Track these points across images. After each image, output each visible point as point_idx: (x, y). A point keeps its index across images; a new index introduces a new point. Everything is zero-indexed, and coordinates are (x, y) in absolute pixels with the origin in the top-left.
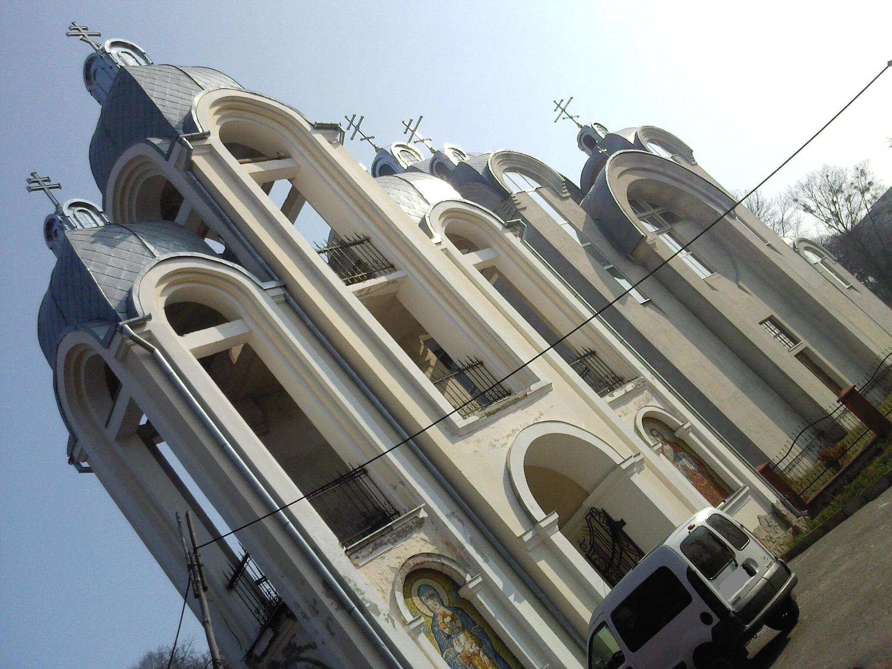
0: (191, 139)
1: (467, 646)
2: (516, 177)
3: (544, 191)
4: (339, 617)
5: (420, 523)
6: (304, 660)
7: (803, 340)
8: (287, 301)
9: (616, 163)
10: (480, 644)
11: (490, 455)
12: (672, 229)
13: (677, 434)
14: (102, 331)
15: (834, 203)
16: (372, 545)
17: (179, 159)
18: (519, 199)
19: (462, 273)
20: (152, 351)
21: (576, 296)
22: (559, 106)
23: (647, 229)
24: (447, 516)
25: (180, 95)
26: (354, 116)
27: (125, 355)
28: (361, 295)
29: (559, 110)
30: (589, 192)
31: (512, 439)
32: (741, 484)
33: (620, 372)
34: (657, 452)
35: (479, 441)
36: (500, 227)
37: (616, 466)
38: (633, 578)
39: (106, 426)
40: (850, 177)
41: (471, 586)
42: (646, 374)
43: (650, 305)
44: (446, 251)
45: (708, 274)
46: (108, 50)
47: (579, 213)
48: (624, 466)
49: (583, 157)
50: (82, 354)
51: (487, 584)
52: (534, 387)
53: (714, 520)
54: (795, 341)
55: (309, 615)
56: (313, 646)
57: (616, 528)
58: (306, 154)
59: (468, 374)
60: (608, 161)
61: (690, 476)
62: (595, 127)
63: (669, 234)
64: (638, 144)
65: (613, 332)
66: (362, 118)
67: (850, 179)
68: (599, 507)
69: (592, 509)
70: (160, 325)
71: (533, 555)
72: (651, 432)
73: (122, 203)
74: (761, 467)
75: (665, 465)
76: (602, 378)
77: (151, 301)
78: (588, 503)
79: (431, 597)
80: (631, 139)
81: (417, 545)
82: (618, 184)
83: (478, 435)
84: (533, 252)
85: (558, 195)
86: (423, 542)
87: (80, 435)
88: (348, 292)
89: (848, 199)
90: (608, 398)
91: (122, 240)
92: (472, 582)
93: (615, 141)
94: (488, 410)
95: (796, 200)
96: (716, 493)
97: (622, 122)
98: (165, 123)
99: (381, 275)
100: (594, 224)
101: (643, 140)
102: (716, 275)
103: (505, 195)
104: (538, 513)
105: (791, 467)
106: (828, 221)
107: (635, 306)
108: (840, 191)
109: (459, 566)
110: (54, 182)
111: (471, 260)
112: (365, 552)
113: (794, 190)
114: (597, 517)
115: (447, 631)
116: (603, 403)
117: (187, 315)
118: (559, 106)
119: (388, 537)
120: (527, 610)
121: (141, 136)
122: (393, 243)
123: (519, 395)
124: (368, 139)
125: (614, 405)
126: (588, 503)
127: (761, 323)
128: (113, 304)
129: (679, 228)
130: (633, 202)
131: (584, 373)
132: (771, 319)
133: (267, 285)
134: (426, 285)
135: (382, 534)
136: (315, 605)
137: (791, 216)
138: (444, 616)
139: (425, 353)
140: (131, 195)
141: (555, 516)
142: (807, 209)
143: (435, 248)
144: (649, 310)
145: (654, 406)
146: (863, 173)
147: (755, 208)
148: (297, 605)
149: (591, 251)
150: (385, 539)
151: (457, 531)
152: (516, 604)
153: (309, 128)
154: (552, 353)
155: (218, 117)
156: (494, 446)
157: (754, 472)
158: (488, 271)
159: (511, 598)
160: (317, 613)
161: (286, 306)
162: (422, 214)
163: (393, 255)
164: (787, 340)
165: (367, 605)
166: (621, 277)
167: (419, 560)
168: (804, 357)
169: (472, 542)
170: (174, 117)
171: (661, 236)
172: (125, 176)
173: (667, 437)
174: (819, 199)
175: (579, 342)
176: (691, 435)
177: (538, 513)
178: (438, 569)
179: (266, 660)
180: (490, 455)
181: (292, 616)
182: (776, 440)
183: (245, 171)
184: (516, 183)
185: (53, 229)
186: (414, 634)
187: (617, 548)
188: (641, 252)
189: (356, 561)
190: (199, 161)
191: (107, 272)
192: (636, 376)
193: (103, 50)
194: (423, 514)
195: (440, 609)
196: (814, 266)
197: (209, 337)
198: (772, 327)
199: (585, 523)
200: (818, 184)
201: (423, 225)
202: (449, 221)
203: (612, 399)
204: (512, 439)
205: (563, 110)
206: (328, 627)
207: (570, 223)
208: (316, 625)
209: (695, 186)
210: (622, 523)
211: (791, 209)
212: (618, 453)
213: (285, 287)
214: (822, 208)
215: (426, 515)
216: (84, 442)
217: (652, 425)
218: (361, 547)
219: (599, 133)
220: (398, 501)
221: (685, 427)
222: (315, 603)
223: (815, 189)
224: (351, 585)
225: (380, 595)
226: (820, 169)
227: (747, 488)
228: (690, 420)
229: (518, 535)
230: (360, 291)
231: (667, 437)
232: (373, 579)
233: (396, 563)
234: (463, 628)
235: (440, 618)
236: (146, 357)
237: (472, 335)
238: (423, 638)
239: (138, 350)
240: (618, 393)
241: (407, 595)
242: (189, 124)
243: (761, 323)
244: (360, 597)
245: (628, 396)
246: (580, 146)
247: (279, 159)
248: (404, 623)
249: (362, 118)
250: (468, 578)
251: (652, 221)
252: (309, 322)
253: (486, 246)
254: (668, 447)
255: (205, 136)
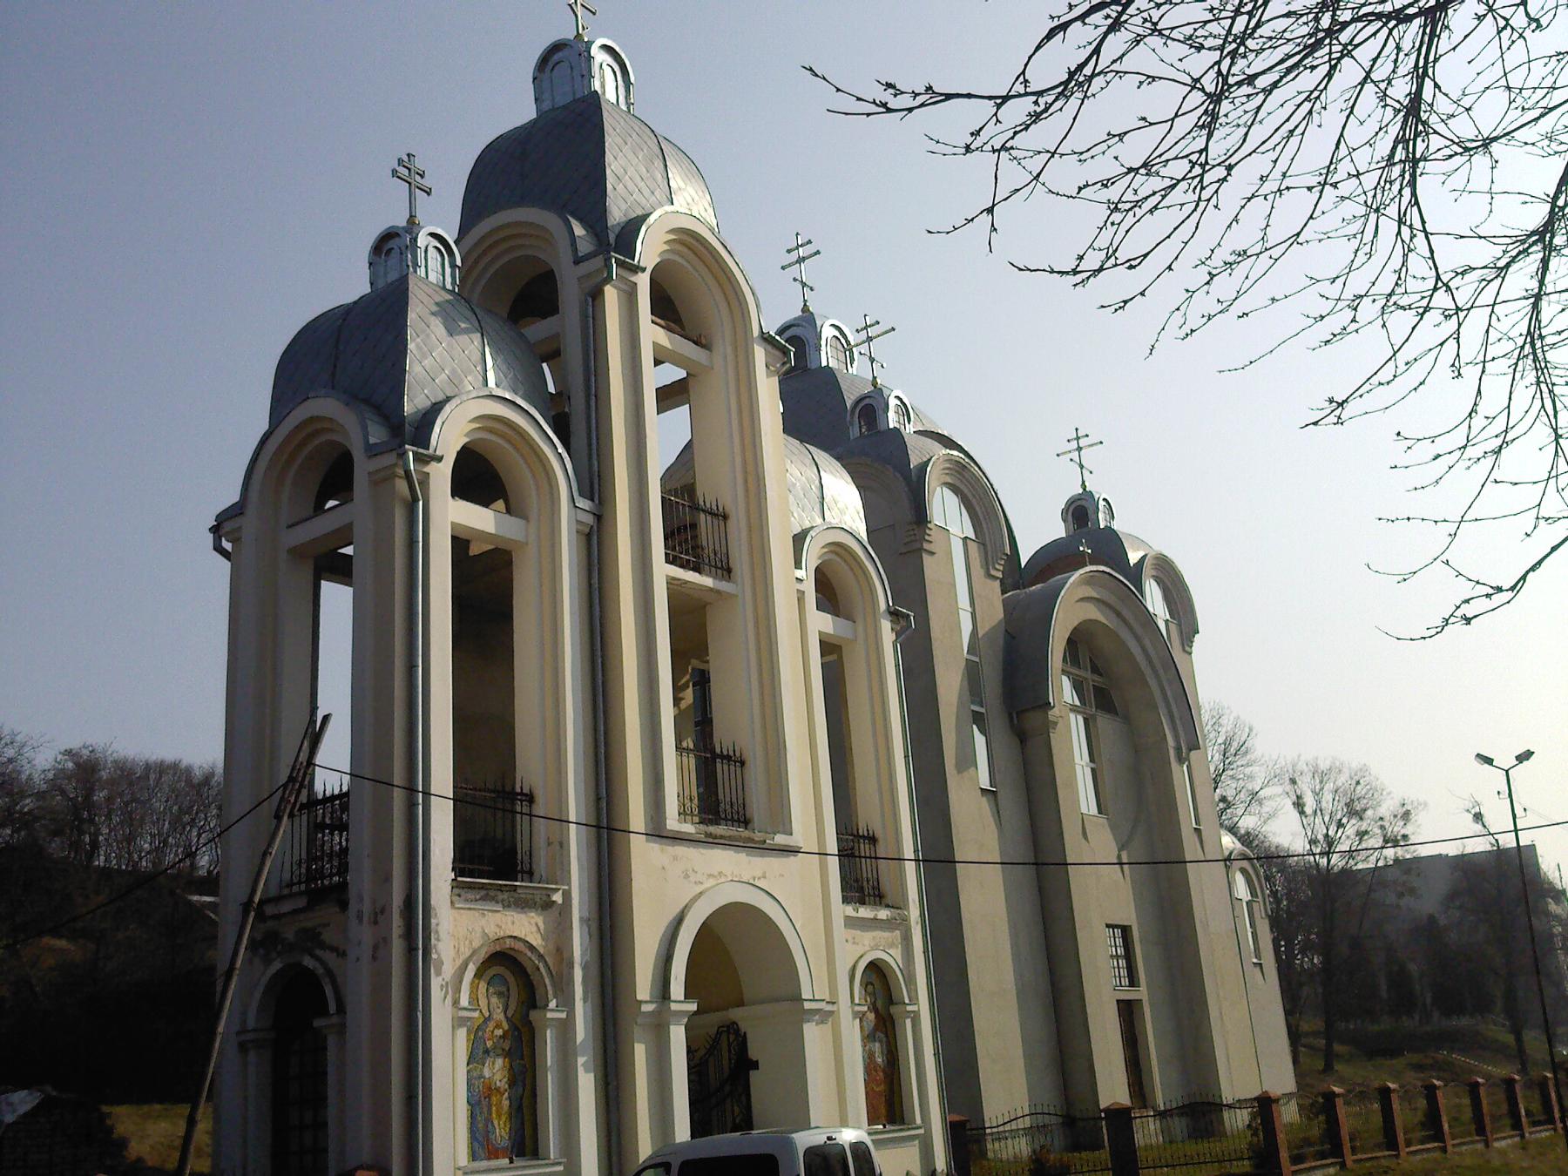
0: (620, 264)
1: (498, 1077)
2: (952, 500)
3: (973, 547)
4: (397, 947)
5: (548, 905)
6: (318, 959)
7: (1143, 988)
8: (589, 536)
9: (1090, 580)
10: (512, 1083)
11: (679, 883)
12: (1093, 717)
13: (893, 1009)
14: (377, 434)
15: (1340, 825)
16: (483, 893)
17: (589, 275)
18: (934, 534)
19: (798, 626)
20: (415, 500)
21: (906, 757)
22: (1078, 438)
23: (1063, 691)
24: (581, 919)
25: (642, 184)
26: (810, 242)
27: (382, 480)
28: (672, 582)
29: (1074, 445)
30: (1027, 581)
31: (712, 882)
32: (919, 1121)
33: (886, 886)
34: (855, 1014)
35: (675, 858)
36: (883, 606)
37: (798, 999)
38: (726, 1143)
39: (289, 527)
40: (1386, 808)
41: (549, 1015)
42: (914, 913)
43: (991, 796)
44: (801, 595)
45: (1094, 810)
46: (594, 50)
47: (994, 612)
48: (807, 1005)
49: (1056, 530)
50: (331, 430)
51: (567, 1026)
52: (780, 839)
53: (860, 1150)
54: (1133, 982)
55: (365, 919)
56: (342, 954)
57: (745, 1064)
58: (730, 358)
59: (719, 766)
60: (1082, 571)
61: (870, 1067)
62: (1102, 503)
63: (1086, 721)
64: (1136, 574)
65: (914, 833)
66: (818, 253)
67: (1384, 810)
68: (743, 1027)
69: (734, 1023)
70: (441, 475)
71: (637, 1030)
72: (866, 984)
73: (485, 253)
74: (957, 1118)
75: (852, 1035)
76: (862, 882)
77: (449, 437)
78: (736, 1014)
79: (500, 994)
80: (1133, 557)
81: (526, 927)
82: (1073, 604)
83: (681, 850)
84: (897, 665)
85: (987, 565)
86: (534, 929)
87: (251, 510)
88: (663, 571)
89: (1362, 835)
90: (849, 910)
91: (466, 331)
92: (553, 1011)
93: (1109, 547)
94: (712, 829)
95: (1293, 781)
96: (883, 1110)
97: (1141, 527)
98: (603, 212)
99: (709, 575)
100: (1001, 641)
101: (1148, 570)
102: (1103, 820)
103: (920, 516)
104: (677, 989)
105: (999, 1137)
106: (1313, 842)
107: (975, 770)
108: (1359, 815)
109: (554, 985)
110: (426, 182)
111: (822, 623)
112: (470, 896)
113: (1301, 766)
114: (732, 1037)
115: (489, 1044)
116: (841, 910)
117: (477, 477)
118: (1078, 438)
119: (506, 895)
120: (587, 1085)
121: (564, 209)
122: (751, 546)
123: (758, 836)
124: (804, 285)
125: (851, 922)
126: (736, 1014)
127: (1108, 926)
128: (408, 408)
129: (1104, 722)
130: (1072, 642)
131: (847, 854)
132: (1126, 931)
133: (583, 503)
134: (751, 625)
135: (500, 888)
136: (380, 913)
137: (1270, 798)
138: (498, 1026)
139: (686, 686)
140: (498, 257)
141: (693, 1007)
142: (1299, 805)
143: (791, 582)
144: (984, 802)
145: (893, 958)
146: (1406, 816)
147: (1232, 750)
148: (361, 899)
149: (973, 673)
150: (501, 896)
151: (579, 944)
152: (581, 1070)
153: (756, 333)
154: (834, 863)
155: (666, 247)
156: (687, 876)
157: (944, 1119)
158: (829, 648)
159: (581, 1060)
160: (376, 923)
161: (583, 538)
162: (807, 525)
163: (740, 559)
164: (1124, 972)
165: (434, 956)
166: (983, 731)
167: (519, 946)
168: (1128, 1011)
169: (585, 968)
170: (617, 212)
171: (1072, 716)
172: (515, 231)
173: (879, 1004)
174: (1324, 805)
175: (868, 816)
176: (908, 1022)
177: (677, 989)
178: (529, 971)
179: (270, 924)
180: (679, 883)
181: (344, 905)
182: (1009, 1092)
183: (652, 334)
184: (947, 513)
185: (391, 247)
186: (459, 1022)
187: (727, 1088)
188: (1032, 720)
189: (456, 898)
190: (611, 294)
191: (426, 362)
192: (899, 905)
193: (589, 44)
194: (557, 898)
195: (499, 1015)
196: (1234, 900)
197: (481, 519)
198: (1119, 941)
199: (713, 1031)
200: (1339, 783)
201: (799, 539)
202: (833, 557)
203: (854, 914)
204: (712, 882)
205: (1079, 449)
206: (375, 948)
207: (973, 615)
208: (363, 934)
209: (1165, 684)
210: (755, 1065)
211: (1279, 790)
212: (812, 987)
213: (599, 518)
214: (1318, 820)
215: (560, 901)
216: (249, 524)
217: (874, 978)
218: (470, 887)
219: (1101, 516)
220: (541, 864)
221: (909, 1008)
222: (382, 912)
223: (1329, 786)
224: (433, 921)
225: (452, 953)
226: (1354, 765)
227: (922, 1131)
228: (920, 1003)
229: (639, 998)
230: (674, 579)
231: (879, 1004)
232: (460, 928)
233: (493, 932)
234: (508, 1054)
235: (491, 1025)
236: (404, 500)
237: (757, 720)
238: (462, 1033)
239: (402, 486)
240: (865, 912)
241: (479, 975)
242: (632, 227)
243: (1108, 926)
244: (433, 941)
245: (874, 924)
246: (1065, 512)
247: (695, 343)
248: (456, 1002)
249: (818, 253)
250: (552, 1004)
251: (1078, 686)
252: (595, 580)
253: (849, 617)
254: (871, 1016)
255: (638, 269)
